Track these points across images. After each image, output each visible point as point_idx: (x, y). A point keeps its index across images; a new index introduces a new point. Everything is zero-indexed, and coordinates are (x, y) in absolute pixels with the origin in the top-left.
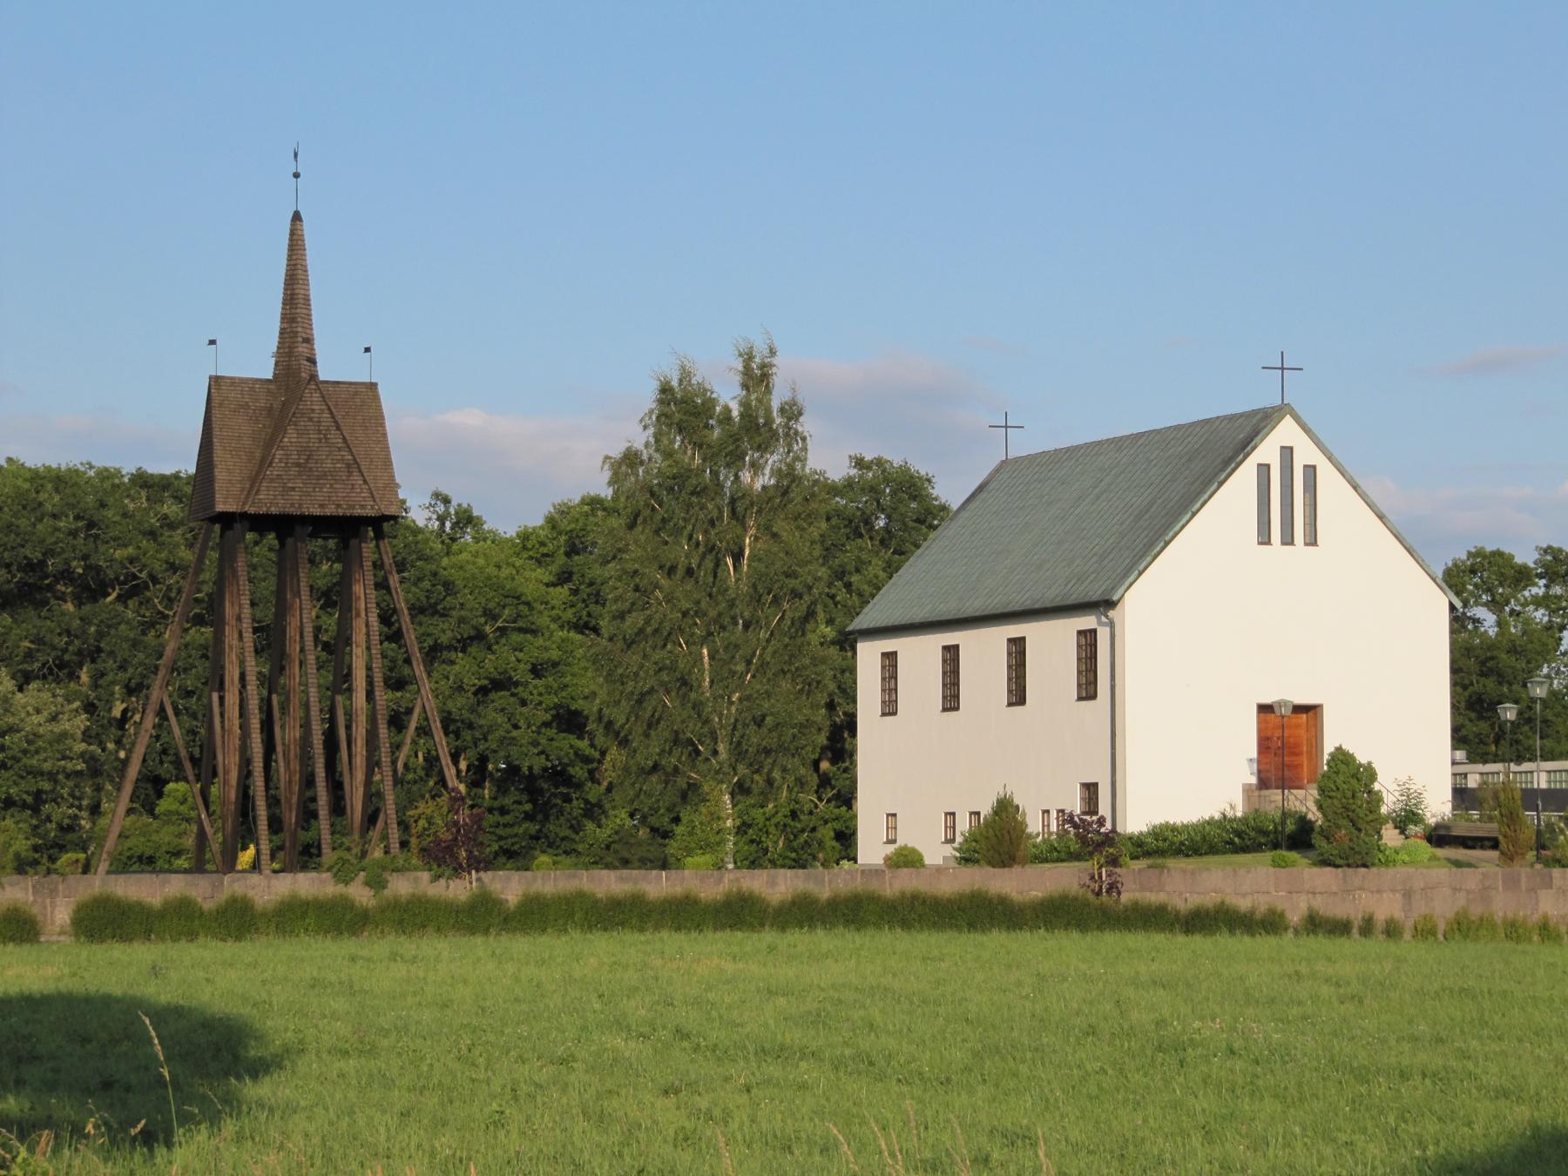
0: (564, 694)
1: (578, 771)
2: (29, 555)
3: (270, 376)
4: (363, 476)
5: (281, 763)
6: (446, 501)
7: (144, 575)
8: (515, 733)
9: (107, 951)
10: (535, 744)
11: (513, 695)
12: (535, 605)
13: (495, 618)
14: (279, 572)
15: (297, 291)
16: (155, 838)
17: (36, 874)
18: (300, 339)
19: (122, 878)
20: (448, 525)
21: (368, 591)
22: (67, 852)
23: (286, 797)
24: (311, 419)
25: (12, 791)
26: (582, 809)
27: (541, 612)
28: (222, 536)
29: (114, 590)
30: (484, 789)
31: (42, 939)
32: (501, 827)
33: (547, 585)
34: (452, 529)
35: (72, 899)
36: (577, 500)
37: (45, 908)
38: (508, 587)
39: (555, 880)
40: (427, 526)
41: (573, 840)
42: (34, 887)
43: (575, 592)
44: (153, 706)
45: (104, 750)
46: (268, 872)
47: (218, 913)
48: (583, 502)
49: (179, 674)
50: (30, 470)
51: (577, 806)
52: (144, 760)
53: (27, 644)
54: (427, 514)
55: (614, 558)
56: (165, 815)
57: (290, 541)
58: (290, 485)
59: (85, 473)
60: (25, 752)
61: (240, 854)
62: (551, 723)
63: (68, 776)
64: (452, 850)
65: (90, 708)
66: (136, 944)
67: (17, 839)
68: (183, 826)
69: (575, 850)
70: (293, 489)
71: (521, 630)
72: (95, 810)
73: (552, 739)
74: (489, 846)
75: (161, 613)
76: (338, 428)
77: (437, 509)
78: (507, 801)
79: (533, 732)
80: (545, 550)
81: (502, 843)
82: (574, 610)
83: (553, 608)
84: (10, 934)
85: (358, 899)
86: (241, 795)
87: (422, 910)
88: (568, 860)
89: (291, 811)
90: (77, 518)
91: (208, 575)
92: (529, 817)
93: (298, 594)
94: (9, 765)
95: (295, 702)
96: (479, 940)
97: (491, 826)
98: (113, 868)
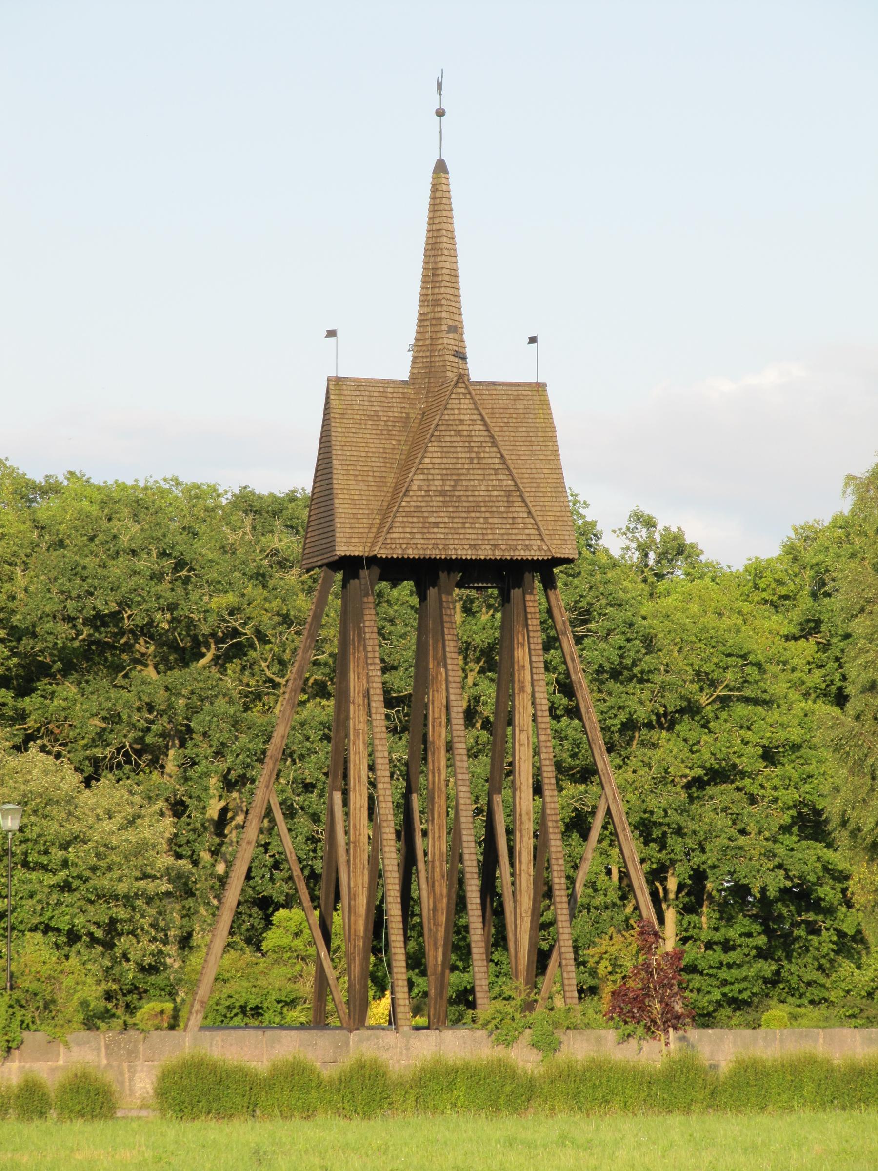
0: (807, 787)
1: (827, 892)
2: (99, 606)
3: (406, 376)
4: (527, 506)
5: (424, 885)
6: (650, 524)
7: (248, 630)
8: (742, 840)
9: (199, 1131)
10: (770, 855)
11: (738, 789)
12: (767, 666)
13: (713, 684)
15: (440, 265)
16: (263, 982)
17: (109, 1029)
18: (445, 328)
19: (219, 1035)
20: (652, 556)
21: (534, 659)
22: (150, 1000)
23: (430, 930)
24: (459, 433)
25: (76, 921)
26: (834, 943)
27: (775, 676)
28: (344, 586)
29: (208, 649)
30: (699, 915)
31: (119, 1115)
32: (724, 968)
33: (787, 638)
34: (658, 561)
35: (156, 1063)
36: (827, 521)
37: (122, 1074)
38: (730, 642)
39: (781, 1041)
40: (623, 558)
41: (823, 986)
42: (107, 1047)
43: (825, 647)
44: (257, 810)
45: (195, 863)
46: (406, 1029)
47: (341, 1081)
48: (835, 525)
49: (294, 762)
50: (99, 488)
51: (826, 941)
52: (248, 877)
53: (96, 721)
54: (623, 542)
55: (862, 610)
56: (274, 952)
57: (432, 592)
58: (433, 520)
59: (170, 491)
60: (94, 869)
61: (373, 1004)
62: (791, 826)
63: (149, 901)
64: (643, 1002)
65: (178, 808)
66: (236, 1122)
67: (84, 983)
68: (298, 967)
69: (826, 1000)
70: (436, 525)
71: (747, 700)
72: (185, 942)
73: (792, 850)
74: (709, 992)
75: (271, 680)
76: (494, 444)
77: (638, 535)
78: (732, 933)
79: (767, 839)
80: (783, 591)
81: (726, 990)
82: (823, 671)
83: (793, 670)
84: (78, 1107)
85: (521, 1064)
86: (371, 927)
87: (604, 1080)
88: (815, 1013)
89: (436, 949)
90: (163, 554)
91: (331, 632)
92: (762, 954)
93: (443, 662)
94: (74, 886)
95: (440, 803)
96: (676, 1120)
97: (711, 967)
98: (209, 1022)
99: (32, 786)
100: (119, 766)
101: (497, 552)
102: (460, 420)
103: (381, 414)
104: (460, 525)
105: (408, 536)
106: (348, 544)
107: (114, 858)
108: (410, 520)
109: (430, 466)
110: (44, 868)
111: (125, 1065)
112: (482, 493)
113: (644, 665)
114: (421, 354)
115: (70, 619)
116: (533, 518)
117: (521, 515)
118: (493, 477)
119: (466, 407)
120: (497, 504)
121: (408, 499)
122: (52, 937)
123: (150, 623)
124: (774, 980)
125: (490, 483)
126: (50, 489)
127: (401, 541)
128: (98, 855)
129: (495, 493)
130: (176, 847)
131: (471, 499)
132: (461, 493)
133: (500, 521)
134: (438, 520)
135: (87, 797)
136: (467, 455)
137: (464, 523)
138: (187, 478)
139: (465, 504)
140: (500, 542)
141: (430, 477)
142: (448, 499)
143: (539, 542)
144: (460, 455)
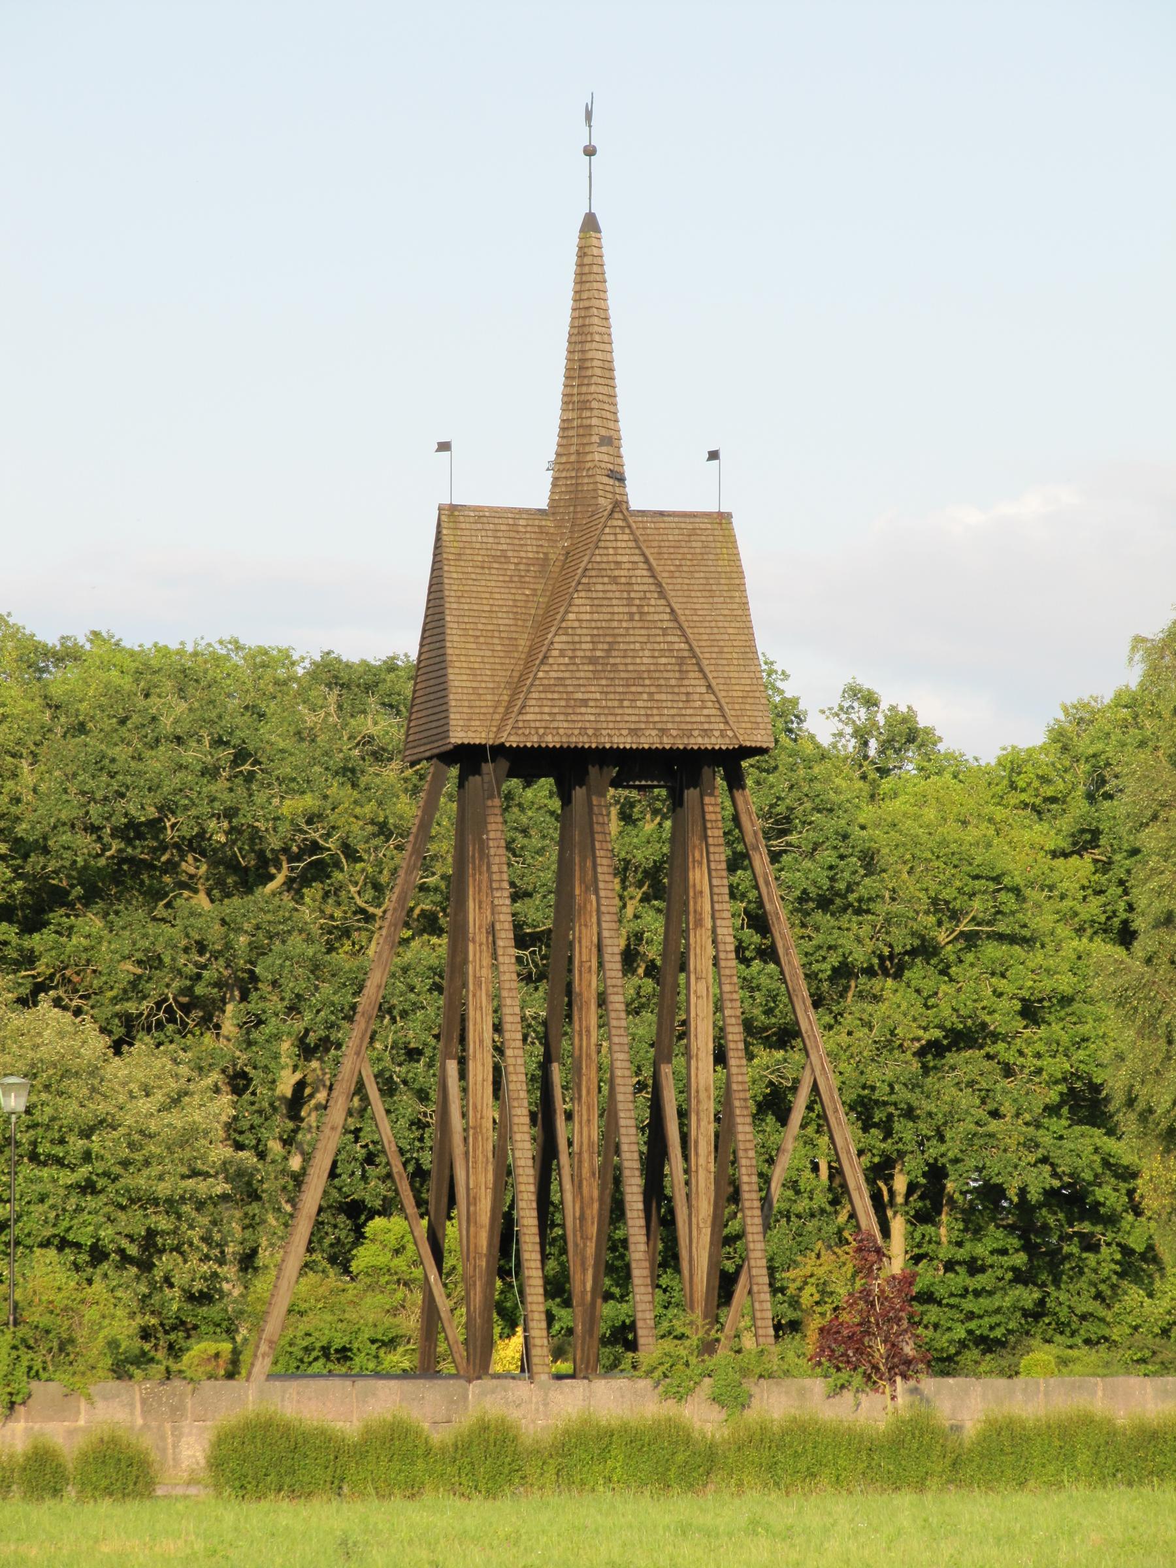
0: (1081, 1054)
1: (1108, 1195)
2: (133, 812)
3: (543, 504)
4: (705, 677)
5: (567, 1186)
6: (870, 701)
7: (332, 844)
8: (994, 1125)
9: (267, 1514)
10: (1031, 1144)
11: (989, 1057)
12: (1028, 892)
13: (955, 916)
14: (562, 835)
15: (590, 355)
16: (352, 1315)
17: (147, 1378)
18: (595, 439)
19: (293, 1386)
20: (873, 744)
21: (715, 882)
22: (200, 1339)
23: (576, 1245)
24: (614, 580)
25: (102, 1234)
26: (1117, 1263)
27: (1038, 905)
28: (461, 785)
29: (279, 870)
30: (936, 1225)
31: (159, 1493)
32: (970, 1297)
33: (1055, 854)
34: (882, 752)
35: (208, 1423)
36: (1108, 698)
37: (163, 1438)
38: (978, 860)
39: (1046, 1394)
40: (835, 747)
41: (1102, 1320)
42: (144, 1402)
43: (1105, 866)
44: (345, 1085)
45: (262, 1156)
46: (544, 1377)
47: (456, 1448)
48: (1118, 703)
49: (394, 1020)
50: (132, 654)
51: (1106, 1260)
52: (333, 1175)
53: (129, 966)
54: (834, 725)
55: (1155, 817)
56: (367, 1274)
57: (579, 793)
58: (580, 696)
59: (227, 658)
60: (125, 1164)
61: (500, 1344)
62: (1059, 1106)
63: (200, 1206)
64: (861, 1341)
65: (239, 1082)
66: (316, 1502)
67: (113, 1317)
68: (399, 1295)
69: (1106, 1339)
70: (585, 702)
71: (1001, 937)
72: (248, 1261)
73: (1061, 1138)
74: (949, 1329)
75: (362, 911)
76: (662, 594)
77: (854, 716)
78: (981, 1250)
79: (1027, 1124)
80: (1049, 791)
81: (972, 1325)
82: (1102, 899)
83: (1063, 897)
84: (104, 1483)
85: (697, 1425)
86: (497, 1241)
87: (809, 1446)
88: (1092, 1356)
89: (584, 1270)
90: (219, 742)
91: (444, 846)
92: (1021, 1277)
93: (593, 886)
94: (99, 1186)
95: (590, 1075)
96: (905, 1500)
97: (952, 1295)
98: (279, 1368)
99: (43, 1052)
100: (160, 1026)
101: (665, 740)
102: (616, 563)
103: (510, 554)
104: (616, 704)
105: (547, 717)
106: (466, 728)
107: (153, 1148)
108: (550, 696)
109: (576, 624)
110: (59, 1162)
111: (168, 1426)
112: (645, 660)
113: (862, 891)
114: (564, 474)
115: (93, 829)
116: (714, 693)
117: (698, 690)
118: (661, 639)
119: (624, 545)
120: (666, 675)
121: (546, 668)
122: (70, 1255)
123: (202, 835)
124: (1037, 1313)
125: (656, 646)
126: (67, 655)
127: (538, 724)
128: (131, 1145)
129: (663, 660)
130: (235, 1134)
131: (631, 668)
132: (618, 660)
133: (670, 697)
134: (586, 696)
135: (117, 1068)
136: (626, 610)
137: (621, 700)
138: (251, 640)
139: (623, 675)
140: (670, 726)
141: (577, 639)
142: (599, 668)
143: (722, 726)
144: (616, 609)
